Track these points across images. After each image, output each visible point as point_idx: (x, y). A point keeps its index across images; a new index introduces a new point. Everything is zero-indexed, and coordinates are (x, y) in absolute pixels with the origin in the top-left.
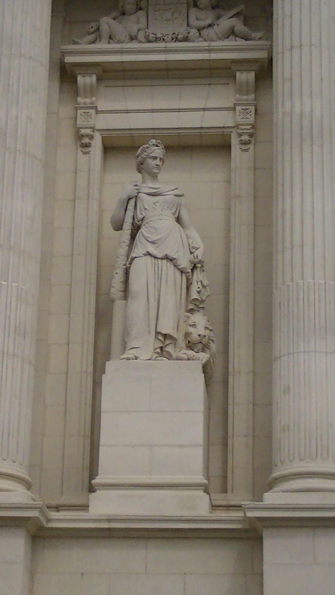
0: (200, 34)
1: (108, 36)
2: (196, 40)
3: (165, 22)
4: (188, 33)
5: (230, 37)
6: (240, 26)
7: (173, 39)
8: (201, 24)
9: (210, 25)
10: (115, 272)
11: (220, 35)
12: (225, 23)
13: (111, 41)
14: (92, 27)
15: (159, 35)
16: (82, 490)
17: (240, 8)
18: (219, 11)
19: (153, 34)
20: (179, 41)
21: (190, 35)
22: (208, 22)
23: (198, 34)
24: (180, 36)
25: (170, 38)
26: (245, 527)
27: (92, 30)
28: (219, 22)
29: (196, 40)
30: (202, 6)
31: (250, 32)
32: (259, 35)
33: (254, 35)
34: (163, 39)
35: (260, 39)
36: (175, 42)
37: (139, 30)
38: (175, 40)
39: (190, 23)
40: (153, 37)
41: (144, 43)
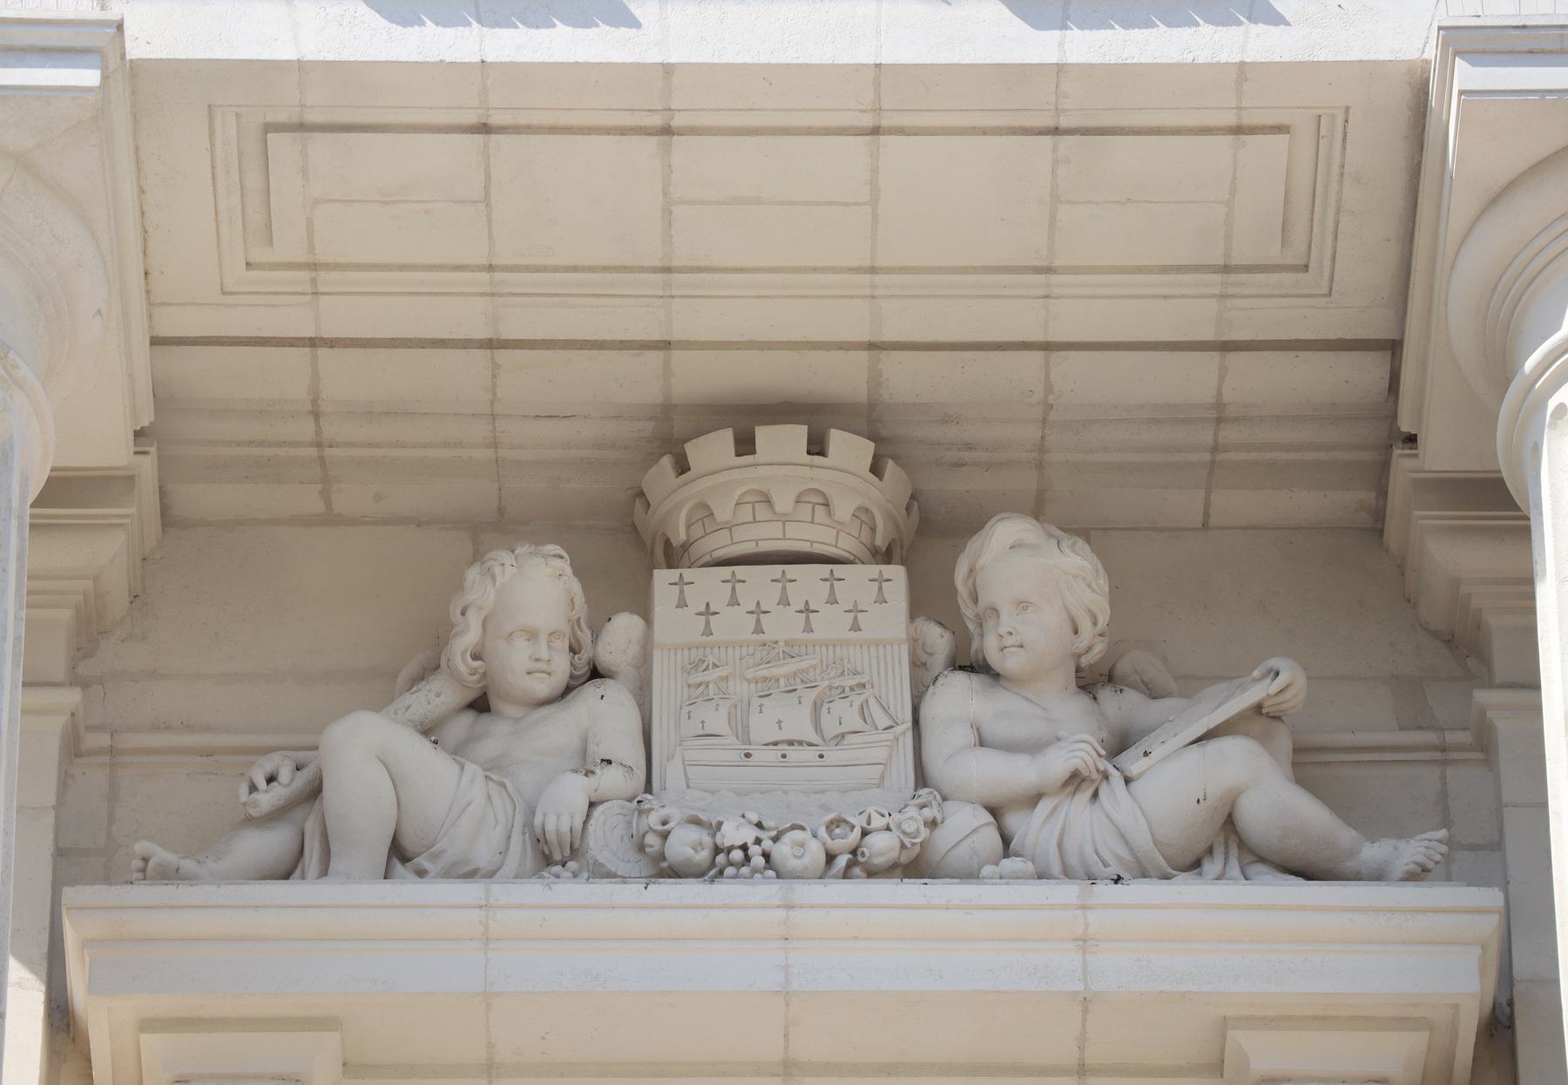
0: (1006, 841)
2: (987, 870)
3: (772, 755)
4: (933, 824)
5: (1212, 867)
6: (1275, 801)
7: (830, 858)
8: (1019, 773)
9: (1075, 780)
10: (1274, 663)
12: (1178, 777)
13: (398, 867)
14: (271, 779)
15: (735, 833)
16: (1416, 456)
17: (1283, 680)
18: (1121, 705)
19: (696, 822)
20: (872, 873)
21: (940, 833)
22: (1057, 764)
23: (992, 838)
24: (882, 846)
25: (815, 853)
26: (1518, 377)
27: (268, 799)
28: (1133, 762)
29: (987, 870)
30: (1009, 663)
31: (1346, 835)
32: (1412, 851)
33: (1372, 853)
34: (766, 856)
35: (1418, 875)
36: (846, 875)
37: (592, 805)
38: (842, 861)
39: (936, 764)
40: (698, 846)
41: (624, 879)
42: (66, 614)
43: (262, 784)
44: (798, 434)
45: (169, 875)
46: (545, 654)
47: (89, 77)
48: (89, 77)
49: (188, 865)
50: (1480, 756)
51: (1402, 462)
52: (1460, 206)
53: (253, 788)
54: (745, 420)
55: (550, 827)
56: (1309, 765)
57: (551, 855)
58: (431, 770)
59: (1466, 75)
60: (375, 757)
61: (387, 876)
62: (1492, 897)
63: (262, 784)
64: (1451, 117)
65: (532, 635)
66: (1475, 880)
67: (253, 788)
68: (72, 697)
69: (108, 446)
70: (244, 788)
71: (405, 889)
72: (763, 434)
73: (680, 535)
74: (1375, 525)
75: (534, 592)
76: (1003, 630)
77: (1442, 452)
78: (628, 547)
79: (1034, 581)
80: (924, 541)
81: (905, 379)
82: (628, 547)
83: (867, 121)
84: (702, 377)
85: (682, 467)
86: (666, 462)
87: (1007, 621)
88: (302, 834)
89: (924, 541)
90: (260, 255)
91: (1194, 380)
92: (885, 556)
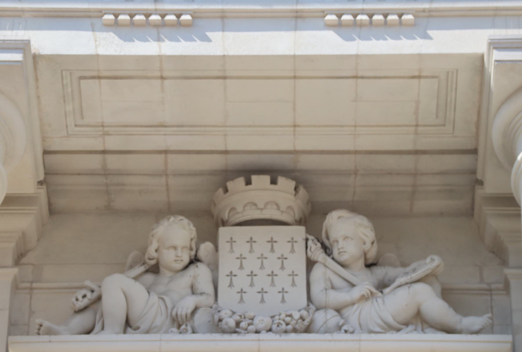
1: (257, 335)
6: (435, 306)
11: (390, 320)
13: (129, 329)
18: (380, 272)
22: (356, 293)
42: (12, 245)
43: (80, 298)
44: (267, 179)
45: (50, 332)
46: (180, 255)
47: (18, 57)
48: (18, 57)
49: (55, 327)
50: (504, 292)
51: (480, 192)
52: (495, 101)
53: (77, 300)
54: (248, 173)
55: (179, 313)
56: (446, 294)
57: (179, 323)
58: (138, 290)
59: (497, 55)
60: (120, 290)
61: (125, 332)
62: (509, 338)
63: (80, 298)
64: (491, 69)
65: (175, 248)
66: (502, 332)
67: (77, 300)
68: (15, 270)
69: (28, 186)
70: (74, 300)
71: (131, 337)
72: (254, 178)
73: (226, 217)
74: (470, 212)
75: (176, 235)
76: (340, 246)
77: (490, 188)
78: (210, 223)
79: (350, 231)
80: (312, 218)
81: (306, 162)
82: (210, 223)
83: (292, 74)
84: (235, 161)
85: (226, 191)
86: (221, 190)
87: (341, 243)
88: (91, 313)
89: (312, 218)
90: (80, 122)
91: (407, 163)
92: (299, 222)
